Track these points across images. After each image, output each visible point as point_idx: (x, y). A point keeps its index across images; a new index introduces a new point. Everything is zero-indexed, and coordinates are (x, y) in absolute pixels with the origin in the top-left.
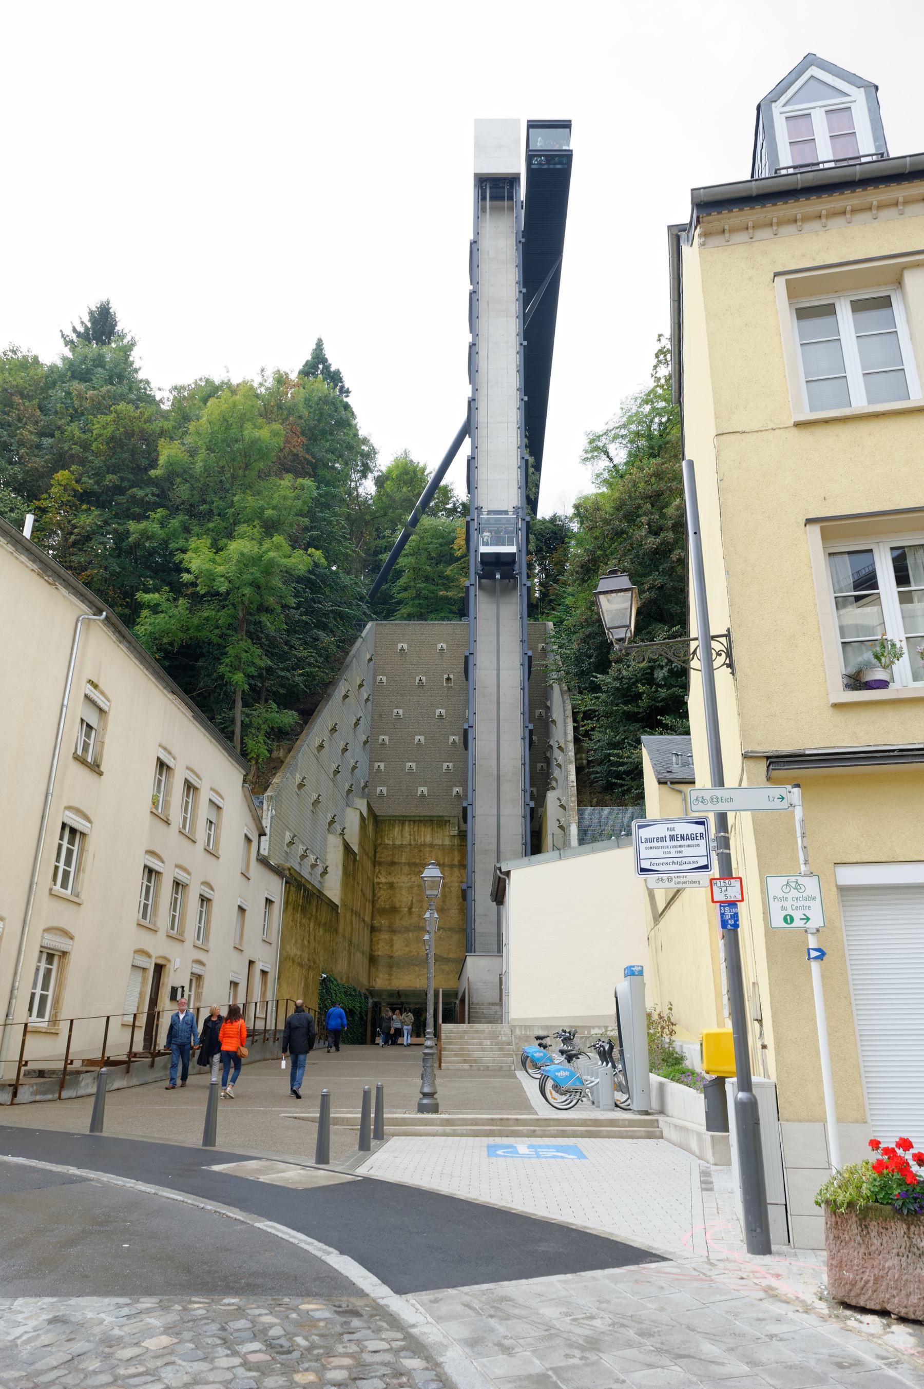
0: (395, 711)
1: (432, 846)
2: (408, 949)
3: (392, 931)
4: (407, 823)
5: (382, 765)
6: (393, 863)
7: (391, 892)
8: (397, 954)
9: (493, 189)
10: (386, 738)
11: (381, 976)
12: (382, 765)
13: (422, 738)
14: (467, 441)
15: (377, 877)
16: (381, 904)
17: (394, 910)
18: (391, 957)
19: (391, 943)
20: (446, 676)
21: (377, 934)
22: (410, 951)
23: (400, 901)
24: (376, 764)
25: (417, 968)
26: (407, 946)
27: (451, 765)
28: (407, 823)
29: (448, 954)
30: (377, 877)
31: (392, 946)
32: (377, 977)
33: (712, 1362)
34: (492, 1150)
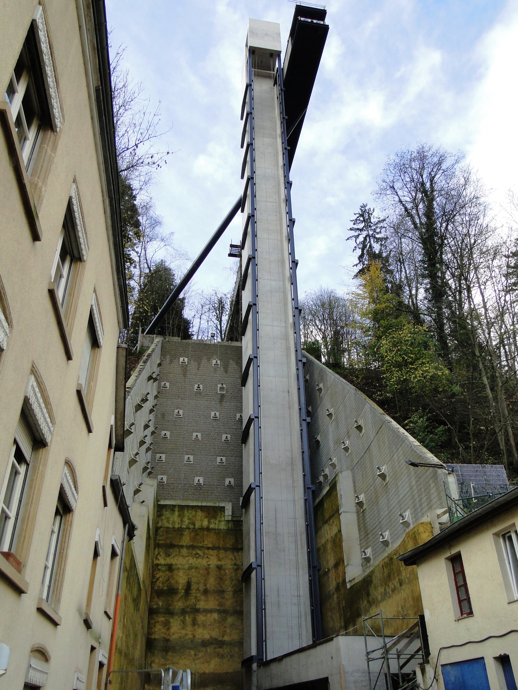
0: (186, 457)
1: (208, 529)
2: (184, 632)
3: (170, 613)
4: (176, 509)
5: (163, 456)
6: (172, 546)
7: (170, 574)
8: (174, 637)
9: (259, 60)
10: (168, 434)
11: (157, 661)
12: (163, 456)
13: (199, 435)
14: (240, 219)
15: (156, 558)
16: (159, 584)
17: (172, 591)
18: (168, 640)
19: (167, 625)
20: (220, 386)
21: (155, 616)
22: (186, 634)
23: (177, 582)
24: (158, 456)
25: (192, 652)
26: (183, 628)
27: (224, 459)
28: (176, 509)
29: (223, 636)
30: (156, 558)
31: (169, 629)
32: (152, 662)
33: (342, 687)
34: (111, 46)
